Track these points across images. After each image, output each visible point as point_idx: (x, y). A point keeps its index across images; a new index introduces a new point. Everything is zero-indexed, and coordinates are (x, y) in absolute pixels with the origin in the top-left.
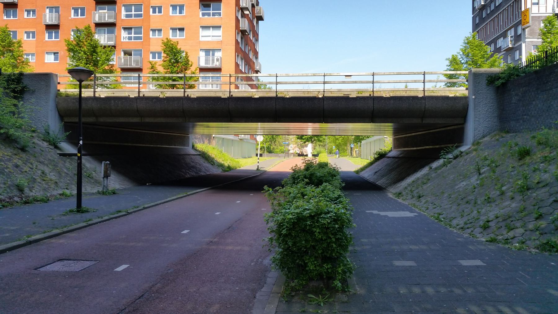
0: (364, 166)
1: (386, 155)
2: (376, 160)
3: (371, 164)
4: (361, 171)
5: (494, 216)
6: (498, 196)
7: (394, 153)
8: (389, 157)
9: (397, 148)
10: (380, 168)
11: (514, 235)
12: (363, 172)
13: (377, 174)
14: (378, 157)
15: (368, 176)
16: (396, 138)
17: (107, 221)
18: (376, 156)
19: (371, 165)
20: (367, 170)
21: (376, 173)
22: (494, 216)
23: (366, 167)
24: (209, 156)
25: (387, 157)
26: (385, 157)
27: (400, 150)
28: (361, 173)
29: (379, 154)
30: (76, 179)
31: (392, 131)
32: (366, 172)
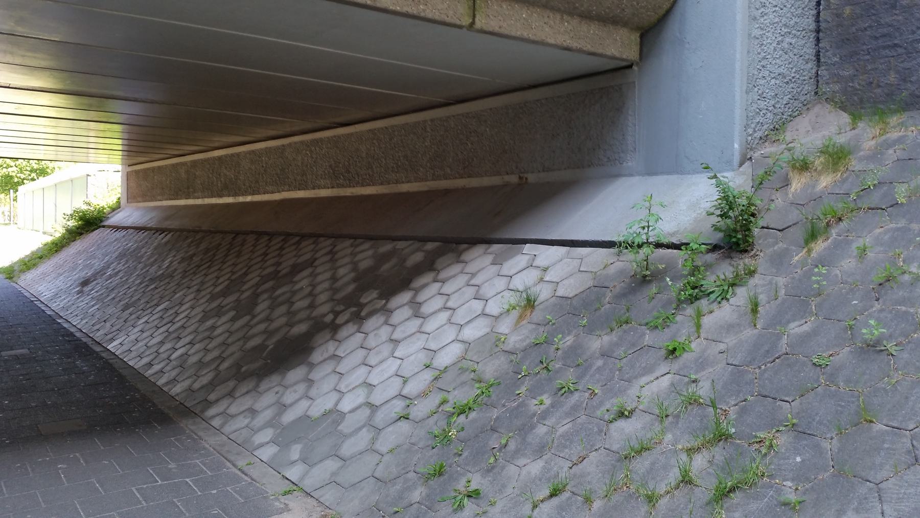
0: (33, 253)
1: (101, 221)
2: (73, 235)
3: (57, 247)
4: (22, 271)
5: (533, 299)
6: (483, 268)
7: (130, 216)
8: (117, 228)
9: (139, 199)
10: (97, 264)
11: (620, 362)
12: (30, 276)
13: (95, 289)
14: (83, 225)
15: (56, 295)
16: (137, 172)
17: (513, 34)
18: (72, 223)
19: (56, 251)
20: (46, 267)
21: (85, 283)
22: (533, 299)
23: (41, 258)
24: (502, 34)
25: (109, 227)
26: (104, 227)
27: (156, 208)
28: (23, 277)
29: (81, 219)
30: (528, 35)
31: (120, 157)
32: (44, 275)
